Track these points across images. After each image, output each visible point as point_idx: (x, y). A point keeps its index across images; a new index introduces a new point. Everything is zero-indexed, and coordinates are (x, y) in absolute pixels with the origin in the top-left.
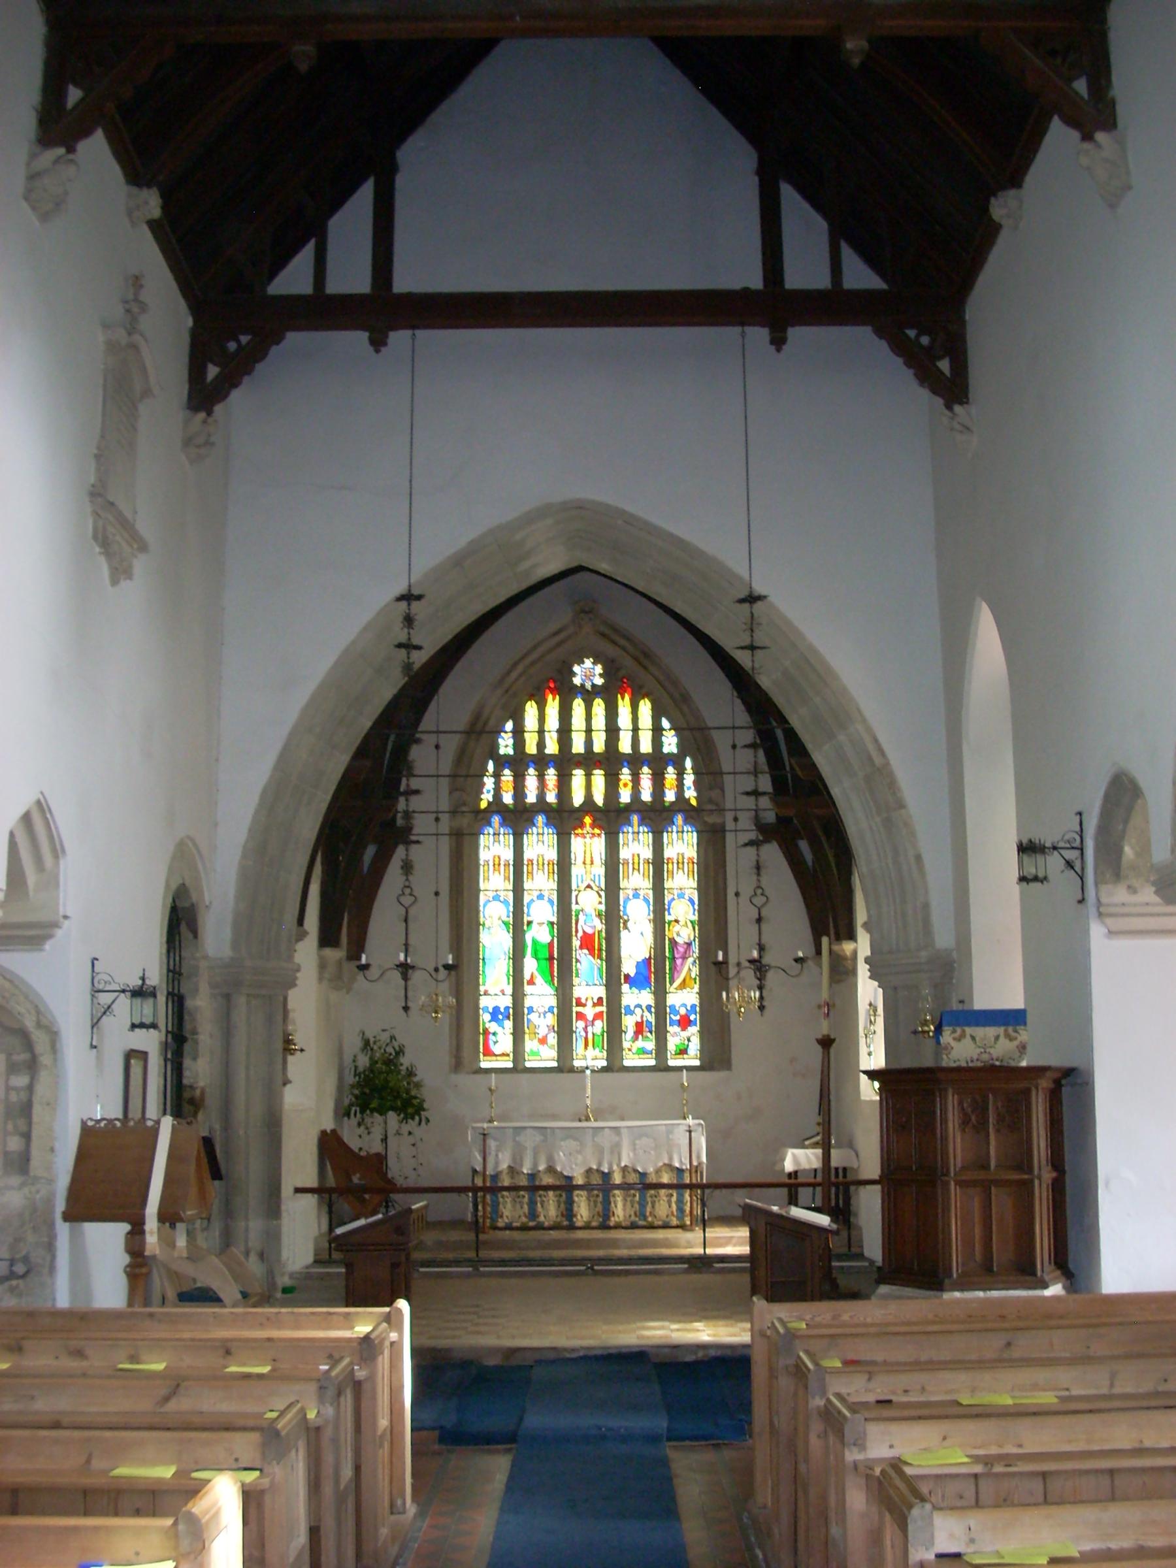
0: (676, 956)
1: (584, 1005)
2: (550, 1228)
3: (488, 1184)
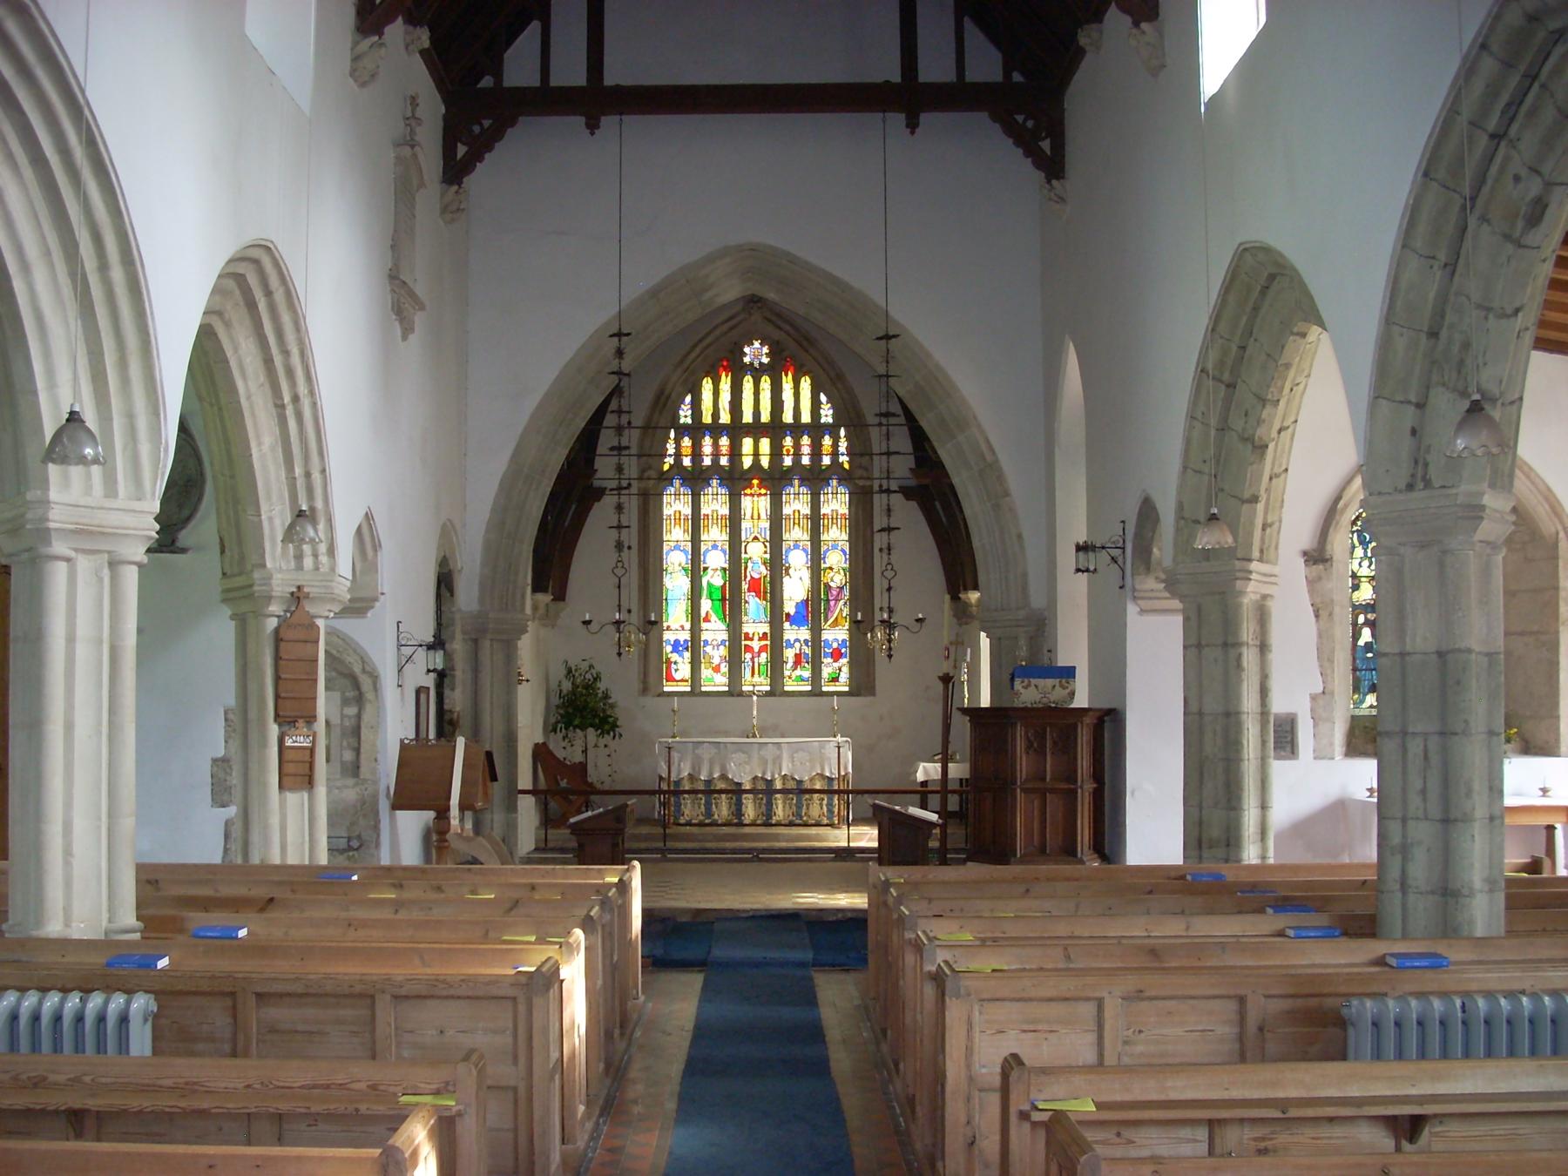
0: (831, 598)
1: (752, 639)
2: (724, 825)
3: (672, 788)
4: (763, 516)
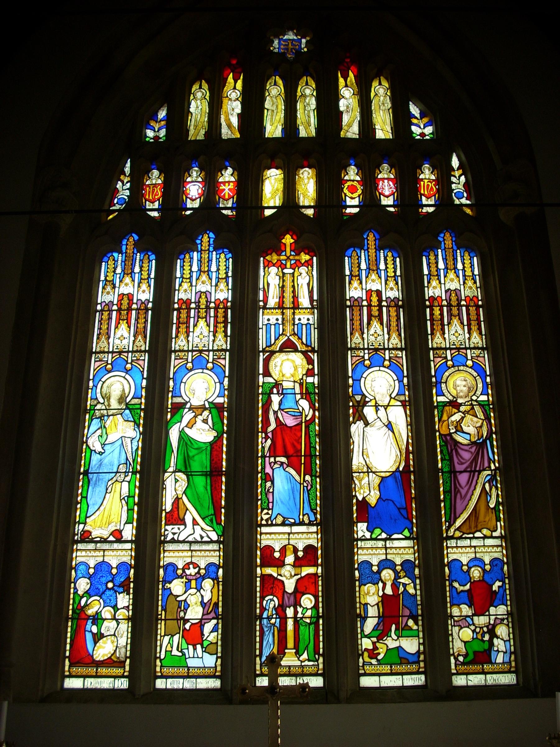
0: (458, 468)
4: (304, 301)
